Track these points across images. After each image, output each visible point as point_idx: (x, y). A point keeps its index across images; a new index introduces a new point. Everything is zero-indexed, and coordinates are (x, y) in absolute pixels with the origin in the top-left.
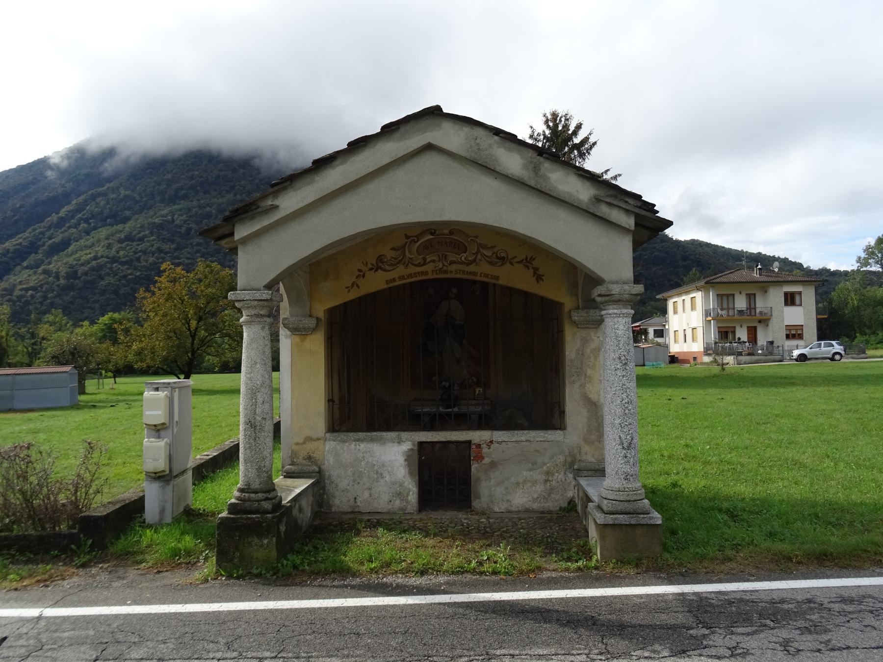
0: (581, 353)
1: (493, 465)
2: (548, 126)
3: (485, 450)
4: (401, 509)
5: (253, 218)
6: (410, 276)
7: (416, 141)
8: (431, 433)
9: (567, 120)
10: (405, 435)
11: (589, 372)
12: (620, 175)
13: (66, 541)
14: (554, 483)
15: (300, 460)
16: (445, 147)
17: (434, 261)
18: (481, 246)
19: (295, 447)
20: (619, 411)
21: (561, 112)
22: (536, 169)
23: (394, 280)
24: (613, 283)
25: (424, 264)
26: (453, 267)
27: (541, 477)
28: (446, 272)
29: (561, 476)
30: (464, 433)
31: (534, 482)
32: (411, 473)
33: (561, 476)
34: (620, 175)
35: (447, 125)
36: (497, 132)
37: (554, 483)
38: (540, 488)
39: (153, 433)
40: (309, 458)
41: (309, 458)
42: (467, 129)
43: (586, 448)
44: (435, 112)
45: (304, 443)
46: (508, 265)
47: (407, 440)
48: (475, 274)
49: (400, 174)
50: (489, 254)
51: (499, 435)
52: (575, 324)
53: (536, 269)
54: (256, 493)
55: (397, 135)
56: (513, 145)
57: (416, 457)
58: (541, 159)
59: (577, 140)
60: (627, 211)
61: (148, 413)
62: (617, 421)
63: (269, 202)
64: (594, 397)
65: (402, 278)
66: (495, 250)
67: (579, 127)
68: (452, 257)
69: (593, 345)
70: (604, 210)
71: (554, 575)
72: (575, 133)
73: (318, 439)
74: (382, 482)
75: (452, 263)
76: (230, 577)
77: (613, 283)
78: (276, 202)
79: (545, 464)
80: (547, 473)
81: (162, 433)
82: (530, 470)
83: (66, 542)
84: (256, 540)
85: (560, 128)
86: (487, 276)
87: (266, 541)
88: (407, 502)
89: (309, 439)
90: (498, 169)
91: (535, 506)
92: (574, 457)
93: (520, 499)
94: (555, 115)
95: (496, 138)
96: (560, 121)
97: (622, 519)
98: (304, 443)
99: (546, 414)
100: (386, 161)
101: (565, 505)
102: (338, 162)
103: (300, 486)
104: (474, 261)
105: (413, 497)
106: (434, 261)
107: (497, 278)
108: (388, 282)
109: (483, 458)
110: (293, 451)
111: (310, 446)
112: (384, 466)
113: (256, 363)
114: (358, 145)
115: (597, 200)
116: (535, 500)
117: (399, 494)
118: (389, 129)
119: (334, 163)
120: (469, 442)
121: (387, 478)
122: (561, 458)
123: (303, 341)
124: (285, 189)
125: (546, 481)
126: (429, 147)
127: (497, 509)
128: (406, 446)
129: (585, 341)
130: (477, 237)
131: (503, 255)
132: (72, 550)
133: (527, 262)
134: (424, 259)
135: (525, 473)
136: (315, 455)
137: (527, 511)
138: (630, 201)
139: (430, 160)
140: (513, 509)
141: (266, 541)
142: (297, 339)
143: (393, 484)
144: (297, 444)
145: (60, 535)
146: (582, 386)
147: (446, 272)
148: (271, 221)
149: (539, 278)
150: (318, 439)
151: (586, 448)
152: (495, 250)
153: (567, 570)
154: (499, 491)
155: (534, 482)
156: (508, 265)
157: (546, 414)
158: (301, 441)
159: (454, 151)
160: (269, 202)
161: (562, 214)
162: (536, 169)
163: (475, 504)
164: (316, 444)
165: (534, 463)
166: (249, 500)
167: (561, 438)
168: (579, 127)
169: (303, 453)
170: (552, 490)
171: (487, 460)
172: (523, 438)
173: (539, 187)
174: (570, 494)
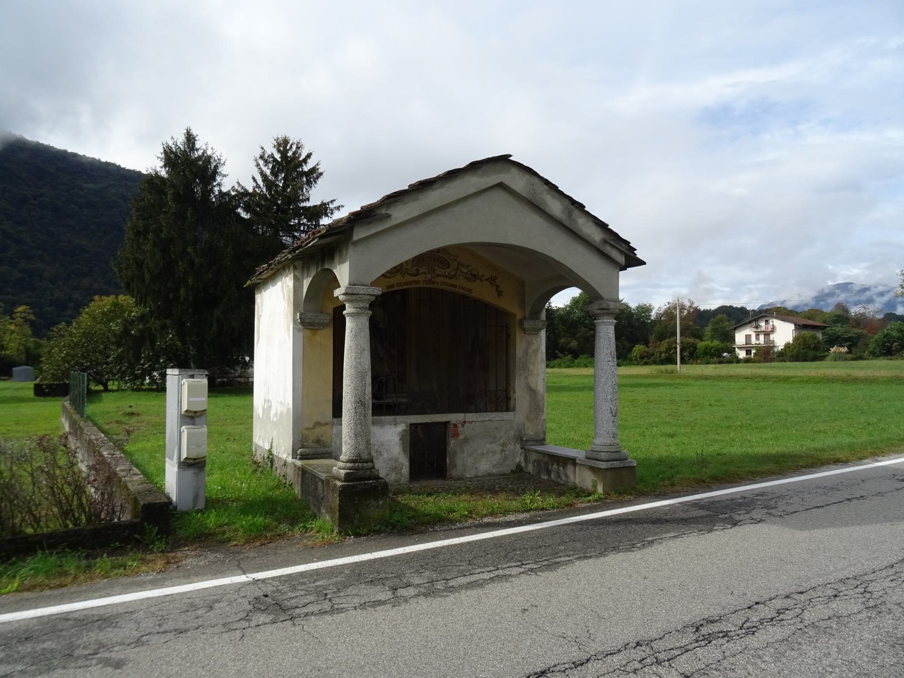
0: (526, 353)
1: (466, 440)
2: (279, 151)
3: (460, 429)
4: (396, 481)
5: (369, 223)
6: (406, 283)
7: (494, 179)
8: (420, 416)
9: (298, 148)
10: (399, 418)
11: (531, 367)
12: (342, 206)
13: (127, 532)
14: (507, 452)
15: (310, 443)
16: (513, 187)
17: (424, 273)
18: (459, 263)
19: (306, 432)
20: (610, 390)
21: (293, 139)
22: (570, 214)
23: (393, 286)
24: (610, 301)
25: (417, 275)
26: (440, 279)
27: (499, 448)
28: (433, 283)
29: (512, 447)
30: (445, 415)
31: (494, 452)
32: (404, 450)
33: (512, 447)
34: (342, 206)
35: (514, 171)
36: (547, 182)
37: (507, 452)
38: (498, 457)
39: (188, 420)
40: (318, 441)
41: (318, 441)
42: (527, 177)
43: (528, 425)
44: (504, 159)
45: (314, 428)
46: (478, 281)
47: (402, 422)
48: (455, 286)
49: (477, 202)
50: (466, 271)
51: (470, 417)
52: (524, 330)
53: (498, 287)
54: (367, 462)
55: (480, 172)
56: (556, 194)
57: (408, 437)
58: (573, 207)
59: (306, 168)
60: (621, 252)
61: (204, 399)
62: (609, 397)
63: (384, 211)
64: (533, 385)
65: (399, 284)
66: (470, 268)
67: (309, 156)
68: (439, 271)
69: (534, 347)
70: (608, 250)
71: (589, 504)
72: (305, 161)
73: (327, 424)
74: (381, 458)
75: (438, 275)
76: (357, 535)
77: (610, 301)
78: (390, 212)
79: (501, 438)
80: (503, 445)
81: (197, 420)
82: (491, 443)
83: (127, 532)
84: (373, 502)
85: (290, 154)
86: (463, 288)
87: (381, 502)
88: (401, 475)
89: (318, 424)
90: (547, 210)
91: (495, 471)
92: (520, 431)
93: (484, 466)
94: (286, 141)
95: (546, 187)
96: (291, 147)
97: (616, 464)
98: (314, 428)
99: (502, 402)
100: (472, 191)
101: (514, 468)
102: (437, 185)
103: (319, 466)
104: (455, 275)
105: (406, 470)
106: (424, 273)
107: (470, 291)
108: (388, 287)
109: (458, 435)
110: (303, 435)
111: (319, 431)
112: (382, 445)
113: (364, 350)
114: (452, 175)
115: (605, 241)
116: (494, 466)
117: (394, 469)
118: (475, 167)
119: (434, 186)
120: (447, 423)
121: (385, 456)
122: (512, 433)
123: (314, 335)
124: (396, 201)
125: (502, 451)
126: (501, 186)
127: (468, 475)
128: (401, 428)
129: (529, 344)
130: (457, 256)
131: (475, 273)
132: (136, 539)
133: (492, 280)
134: (417, 270)
135: (488, 446)
136: (323, 439)
137: (489, 475)
138: (624, 245)
139: (499, 195)
140: (480, 474)
141: (381, 502)
142: (308, 333)
143: (390, 460)
144: (307, 429)
145: (120, 526)
146: (526, 378)
147: (433, 283)
148: (385, 227)
149: (500, 293)
150: (327, 424)
151: (528, 425)
152: (470, 268)
153: (589, 501)
154: (470, 461)
155: (494, 452)
156: (478, 281)
157: (502, 402)
158: (311, 426)
159: (518, 191)
160: (384, 211)
161: (580, 249)
162: (570, 214)
163: (454, 473)
164: (324, 428)
165: (494, 438)
166: (363, 469)
167: (512, 418)
168: (309, 156)
169: (313, 437)
170: (505, 458)
171: (461, 437)
172: (487, 418)
173: (571, 227)
174: (517, 460)
